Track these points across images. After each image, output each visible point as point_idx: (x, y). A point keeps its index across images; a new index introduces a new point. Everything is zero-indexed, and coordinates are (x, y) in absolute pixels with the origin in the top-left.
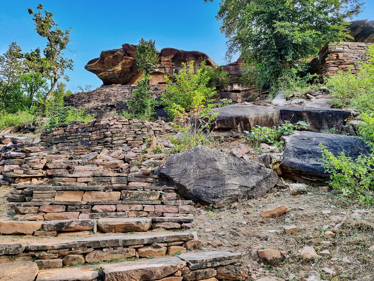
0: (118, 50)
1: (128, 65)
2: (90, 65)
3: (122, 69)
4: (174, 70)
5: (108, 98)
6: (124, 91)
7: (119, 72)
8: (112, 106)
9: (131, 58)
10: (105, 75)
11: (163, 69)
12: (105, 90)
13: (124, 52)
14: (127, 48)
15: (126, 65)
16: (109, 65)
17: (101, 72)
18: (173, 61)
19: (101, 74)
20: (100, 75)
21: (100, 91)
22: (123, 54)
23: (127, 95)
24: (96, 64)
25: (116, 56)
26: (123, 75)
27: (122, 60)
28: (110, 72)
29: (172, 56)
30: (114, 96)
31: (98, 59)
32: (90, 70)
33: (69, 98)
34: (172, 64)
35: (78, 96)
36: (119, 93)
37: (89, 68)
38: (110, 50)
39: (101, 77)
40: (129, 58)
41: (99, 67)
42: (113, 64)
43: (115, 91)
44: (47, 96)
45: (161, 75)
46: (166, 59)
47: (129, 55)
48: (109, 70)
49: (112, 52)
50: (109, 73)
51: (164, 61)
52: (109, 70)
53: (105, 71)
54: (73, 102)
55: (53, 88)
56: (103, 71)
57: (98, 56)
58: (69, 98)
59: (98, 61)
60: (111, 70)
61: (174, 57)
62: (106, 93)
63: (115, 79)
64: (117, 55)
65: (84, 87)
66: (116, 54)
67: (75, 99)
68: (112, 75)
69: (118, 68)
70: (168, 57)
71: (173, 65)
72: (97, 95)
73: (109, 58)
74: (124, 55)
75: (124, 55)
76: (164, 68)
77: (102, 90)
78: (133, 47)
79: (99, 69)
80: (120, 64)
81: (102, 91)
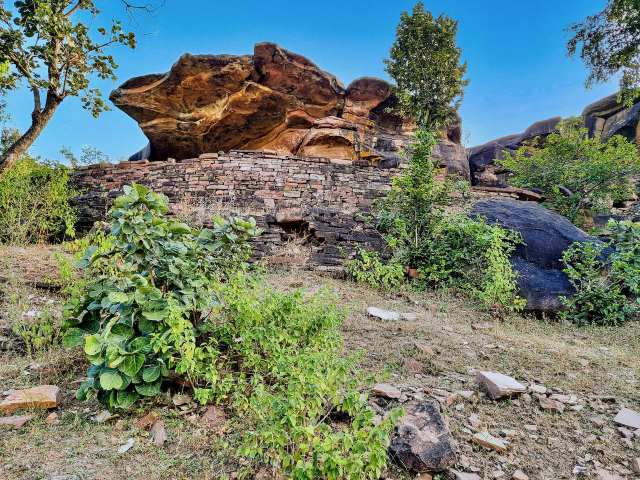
0: (234, 60)
1: (247, 109)
2: (129, 91)
3: (221, 121)
4: (375, 139)
5: (247, 193)
6: (307, 176)
7: (212, 123)
8: (293, 227)
9: (267, 89)
10: (165, 127)
11: (353, 132)
12: (235, 163)
13: (252, 68)
14: (267, 55)
15: (241, 108)
16: (188, 101)
17: (154, 115)
18: (372, 118)
19: (154, 122)
20: (149, 124)
21: (217, 164)
22: (246, 73)
23: (320, 192)
24: (149, 91)
25: (223, 75)
26: (217, 135)
27: (234, 91)
28: (183, 120)
29: (375, 103)
30: (271, 189)
31: (159, 77)
32: (124, 108)
33: (83, 176)
34: (369, 123)
35: (120, 171)
36: (290, 180)
37: (124, 99)
38: (213, 56)
39: (151, 130)
40: (261, 87)
41: (156, 100)
42: (200, 100)
43: (275, 174)
44: (12, 156)
45: (342, 148)
46: (357, 108)
47: (263, 80)
48: (182, 115)
49: (216, 63)
50: (178, 124)
51: (352, 113)
52: (182, 115)
53: (168, 116)
54: (98, 189)
55: (38, 128)
56: (163, 116)
57: (165, 69)
58: (83, 176)
59: (159, 83)
60: (187, 115)
61: (379, 105)
62: (240, 176)
63: (188, 143)
64: (228, 73)
65: (78, 154)
66: (224, 69)
67: (109, 180)
68: (186, 129)
69: (212, 113)
70: (363, 104)
71: (371, 127)
72: (205, 177)
73: (199, 80)
74: (249, 78)
75: (249, 78)
76: (354, 129)
77: (223, 162)
78: (286, 58)
79: (153, 105)
80: (224, 101)
81: (225, 165)
